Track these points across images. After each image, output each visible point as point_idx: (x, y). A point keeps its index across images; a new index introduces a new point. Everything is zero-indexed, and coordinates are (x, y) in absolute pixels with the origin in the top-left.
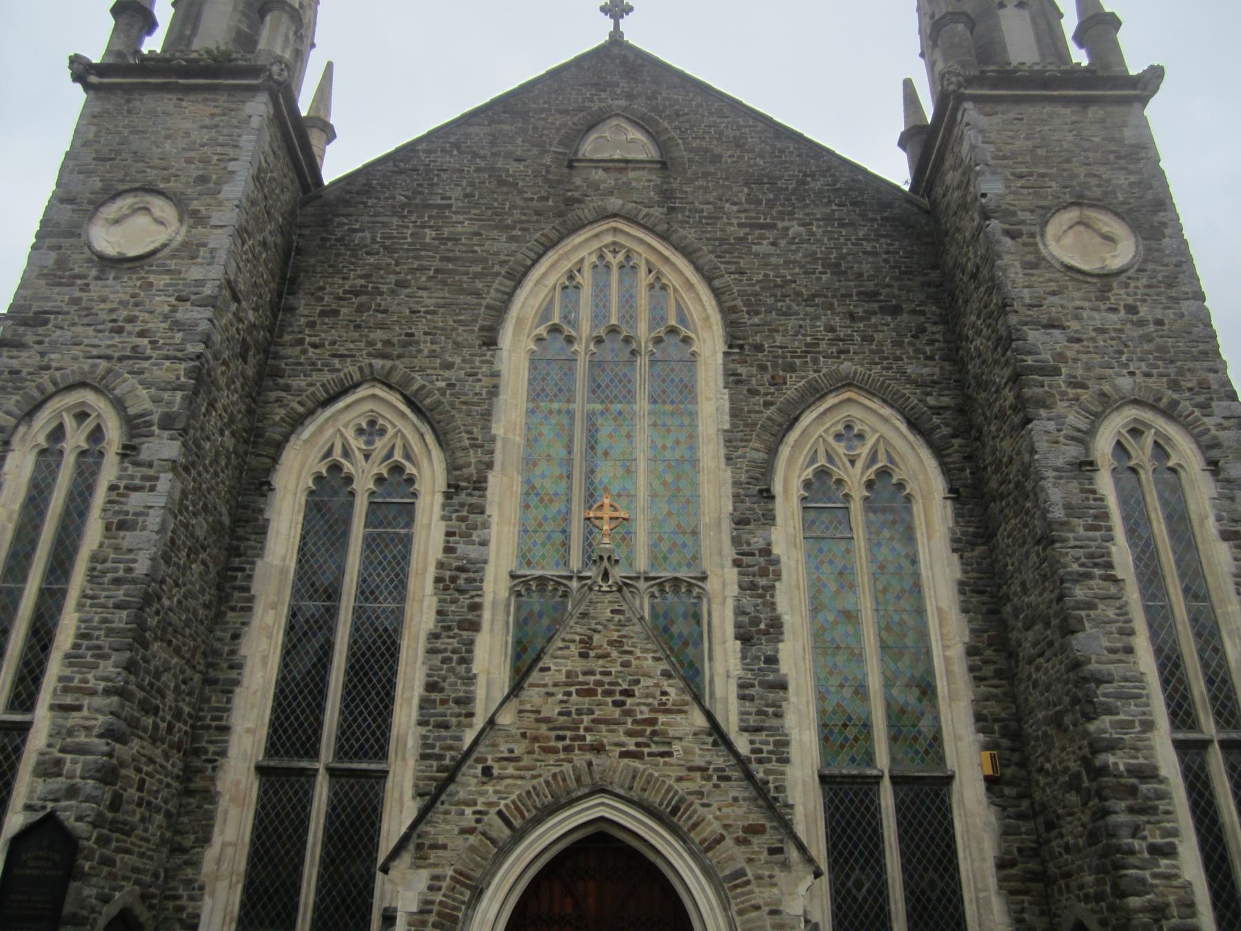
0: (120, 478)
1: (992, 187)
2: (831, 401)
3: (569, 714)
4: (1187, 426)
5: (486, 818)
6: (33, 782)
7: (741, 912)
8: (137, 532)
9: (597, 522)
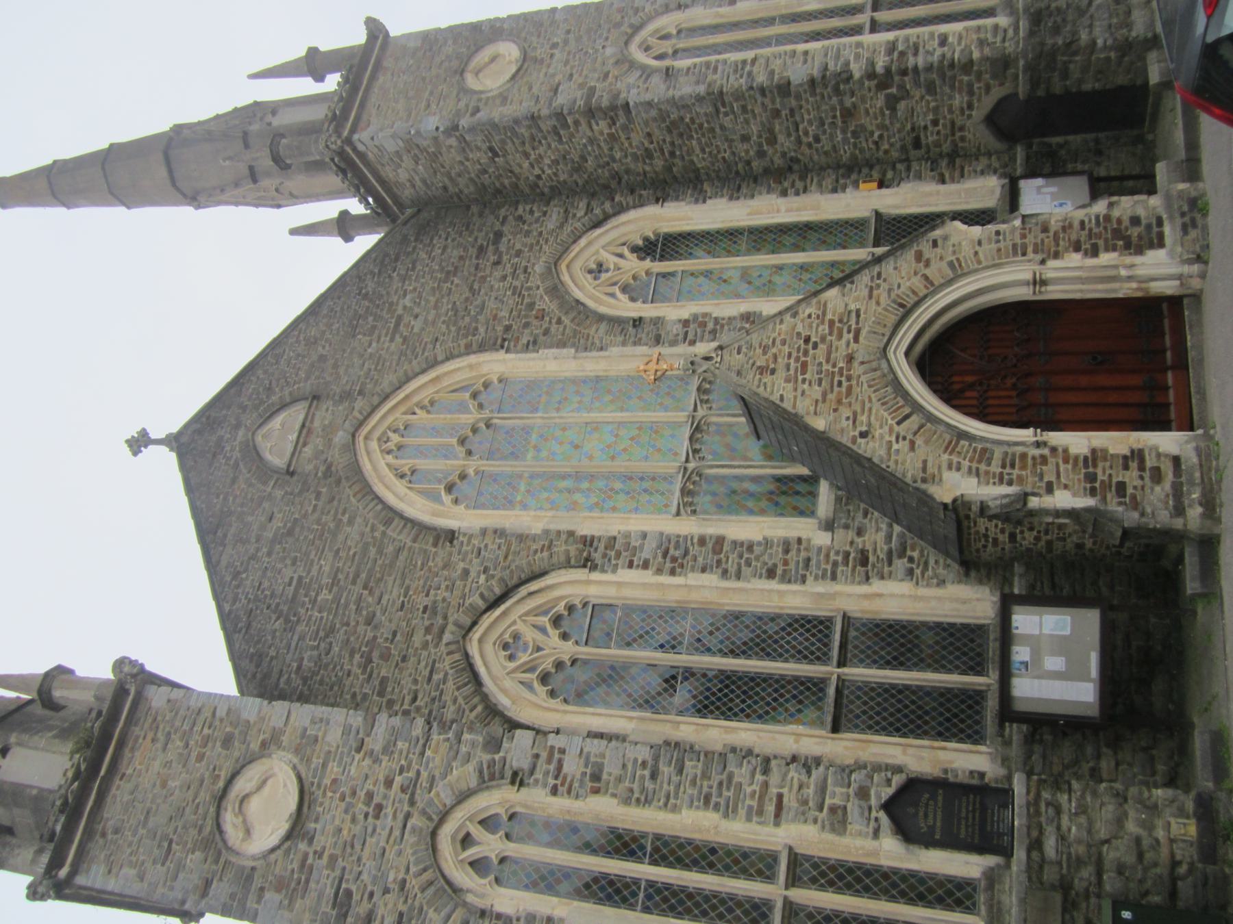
0: (545, 785)
1: (431, 123)
2: (566, 278)
3: (820, 381)
4: (650, 18)
5: (902, 434)
6: (851, 834)
7: (979, 262)
8: (606, 762)
9: (659, 373)
